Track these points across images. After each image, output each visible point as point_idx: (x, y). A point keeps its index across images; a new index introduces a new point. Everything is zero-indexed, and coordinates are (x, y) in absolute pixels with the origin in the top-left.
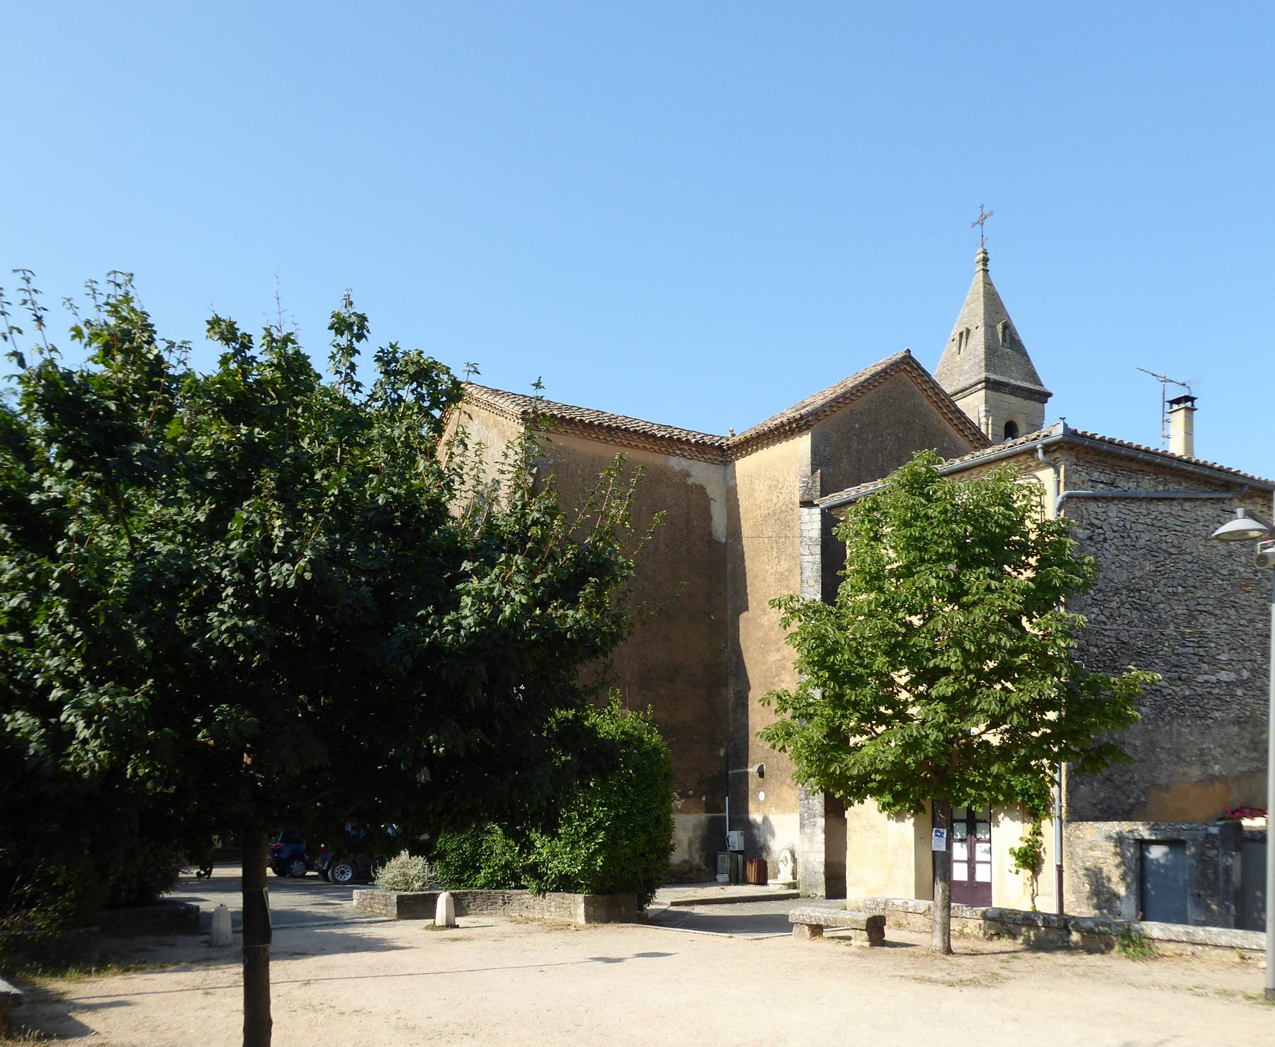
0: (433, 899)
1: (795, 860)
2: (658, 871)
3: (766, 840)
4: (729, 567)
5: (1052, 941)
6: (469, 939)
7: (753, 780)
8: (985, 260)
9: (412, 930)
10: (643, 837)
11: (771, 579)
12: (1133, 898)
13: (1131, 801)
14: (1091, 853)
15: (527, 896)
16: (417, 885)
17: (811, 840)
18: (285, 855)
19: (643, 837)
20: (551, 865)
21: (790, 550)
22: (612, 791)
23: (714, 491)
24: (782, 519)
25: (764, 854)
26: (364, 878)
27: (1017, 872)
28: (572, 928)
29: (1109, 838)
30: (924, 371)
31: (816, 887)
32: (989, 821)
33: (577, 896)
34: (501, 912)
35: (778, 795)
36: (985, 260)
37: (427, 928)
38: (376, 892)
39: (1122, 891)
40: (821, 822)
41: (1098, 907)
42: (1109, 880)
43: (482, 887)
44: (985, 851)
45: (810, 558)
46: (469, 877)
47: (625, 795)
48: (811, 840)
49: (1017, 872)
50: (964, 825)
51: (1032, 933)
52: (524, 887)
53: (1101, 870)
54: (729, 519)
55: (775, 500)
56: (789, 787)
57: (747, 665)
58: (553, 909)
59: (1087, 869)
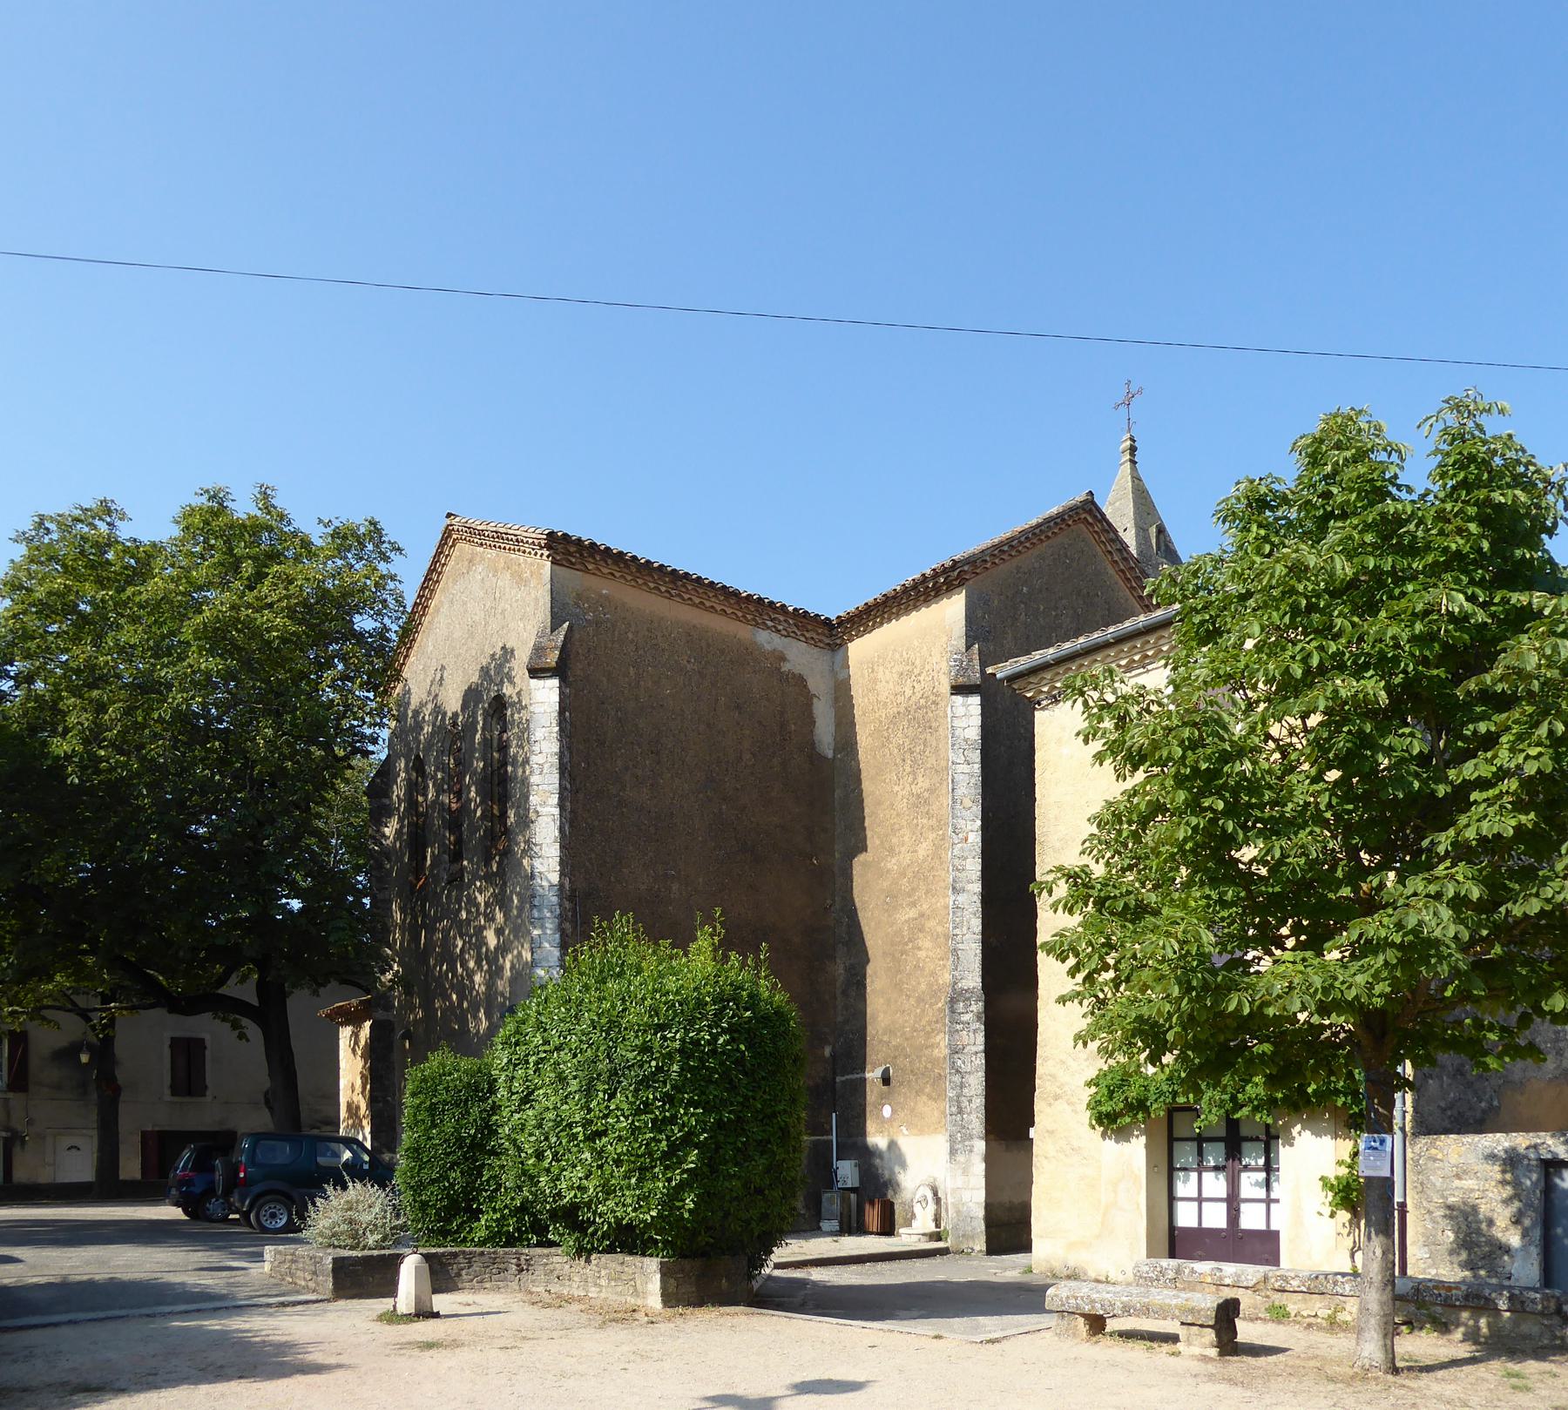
0: (394, 1263)
1: (938, 1201)
2: (783, 1219)
3: (892, 1172)
4: (838, 793)
5: (1525, 1337)
6: (455, 1344)
7: (873, 1090)
8: (1133, 450)
9: (355, 1320)
10: (762, 1162)
11: (902, 805)
12: (1534, 1251)
13: (1483, 1104)
14: (1457, 1183)
15: (558, 1259)
16: (372, 1239)
17: (965, 1172)
18: (197, 1190)
19: (762, 1162)
20: (601, 1208)
21: (932, 761)
22: (710, 1081)
23: (818, 684)
24: (921, 718)
25: (890, 1193)
26: (292, 1229)
27: (1332, 1215)
28: (640, 1316)
29: (1491, 1157)
30: (1110, 525)
31: (973, 1237)
32: (1270, 1140)
33: (647, 1260)
34: (514, 1285)
35: (912, 1110)
36: (1133, 450)
37: (380, 1318)
38: (301, 1250)
39: (1514, 1239)
40: (981, 1146)
41: (1469, 1265)
42: (1491, 1222)
43: (482, 1243)
44: (1257, 1184)
45: (966, 768)
46: (460, 1226)
47: (733, 1088)
48: (965, 1172)
49: (1332, 1215)
50: (1221, 1146)
51: (1483, 1322)
52: (552, 1244)
53: (1475, 1209)
54: (838, 725)
55: (909, 692)
56: (930, 1097)
57: (865, 929)
58: (603, 1282)
59: (1449, 1207)
